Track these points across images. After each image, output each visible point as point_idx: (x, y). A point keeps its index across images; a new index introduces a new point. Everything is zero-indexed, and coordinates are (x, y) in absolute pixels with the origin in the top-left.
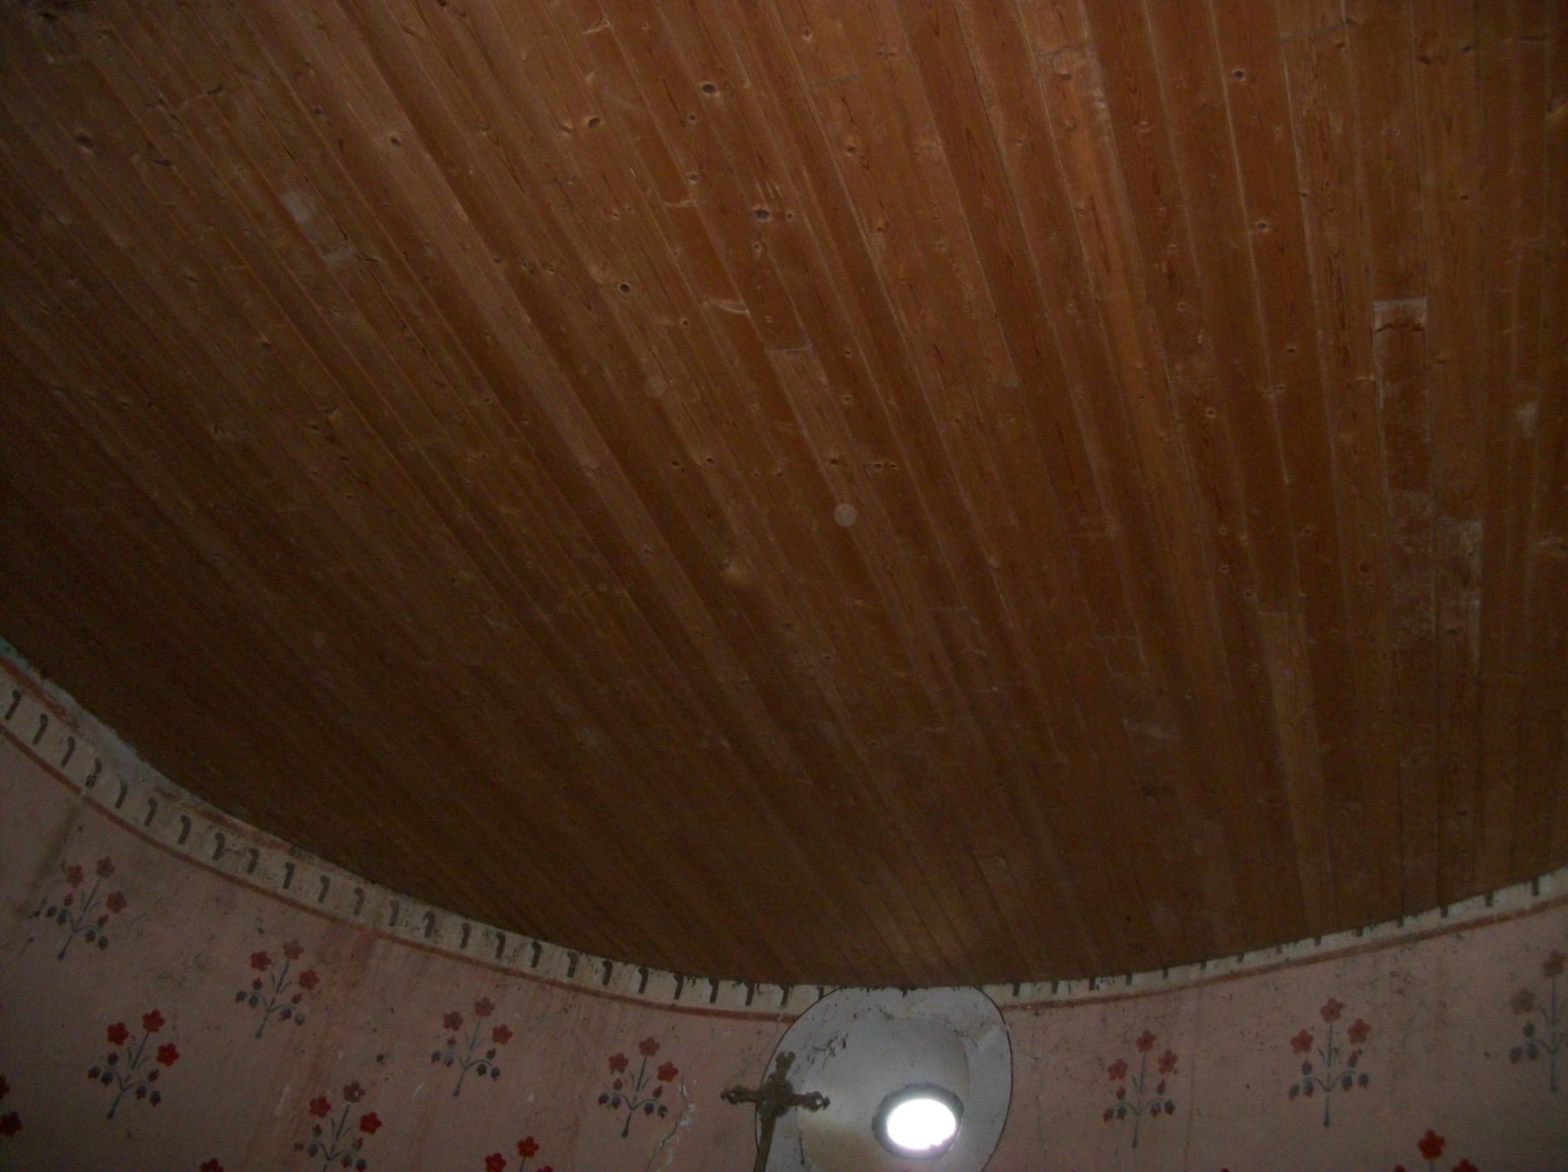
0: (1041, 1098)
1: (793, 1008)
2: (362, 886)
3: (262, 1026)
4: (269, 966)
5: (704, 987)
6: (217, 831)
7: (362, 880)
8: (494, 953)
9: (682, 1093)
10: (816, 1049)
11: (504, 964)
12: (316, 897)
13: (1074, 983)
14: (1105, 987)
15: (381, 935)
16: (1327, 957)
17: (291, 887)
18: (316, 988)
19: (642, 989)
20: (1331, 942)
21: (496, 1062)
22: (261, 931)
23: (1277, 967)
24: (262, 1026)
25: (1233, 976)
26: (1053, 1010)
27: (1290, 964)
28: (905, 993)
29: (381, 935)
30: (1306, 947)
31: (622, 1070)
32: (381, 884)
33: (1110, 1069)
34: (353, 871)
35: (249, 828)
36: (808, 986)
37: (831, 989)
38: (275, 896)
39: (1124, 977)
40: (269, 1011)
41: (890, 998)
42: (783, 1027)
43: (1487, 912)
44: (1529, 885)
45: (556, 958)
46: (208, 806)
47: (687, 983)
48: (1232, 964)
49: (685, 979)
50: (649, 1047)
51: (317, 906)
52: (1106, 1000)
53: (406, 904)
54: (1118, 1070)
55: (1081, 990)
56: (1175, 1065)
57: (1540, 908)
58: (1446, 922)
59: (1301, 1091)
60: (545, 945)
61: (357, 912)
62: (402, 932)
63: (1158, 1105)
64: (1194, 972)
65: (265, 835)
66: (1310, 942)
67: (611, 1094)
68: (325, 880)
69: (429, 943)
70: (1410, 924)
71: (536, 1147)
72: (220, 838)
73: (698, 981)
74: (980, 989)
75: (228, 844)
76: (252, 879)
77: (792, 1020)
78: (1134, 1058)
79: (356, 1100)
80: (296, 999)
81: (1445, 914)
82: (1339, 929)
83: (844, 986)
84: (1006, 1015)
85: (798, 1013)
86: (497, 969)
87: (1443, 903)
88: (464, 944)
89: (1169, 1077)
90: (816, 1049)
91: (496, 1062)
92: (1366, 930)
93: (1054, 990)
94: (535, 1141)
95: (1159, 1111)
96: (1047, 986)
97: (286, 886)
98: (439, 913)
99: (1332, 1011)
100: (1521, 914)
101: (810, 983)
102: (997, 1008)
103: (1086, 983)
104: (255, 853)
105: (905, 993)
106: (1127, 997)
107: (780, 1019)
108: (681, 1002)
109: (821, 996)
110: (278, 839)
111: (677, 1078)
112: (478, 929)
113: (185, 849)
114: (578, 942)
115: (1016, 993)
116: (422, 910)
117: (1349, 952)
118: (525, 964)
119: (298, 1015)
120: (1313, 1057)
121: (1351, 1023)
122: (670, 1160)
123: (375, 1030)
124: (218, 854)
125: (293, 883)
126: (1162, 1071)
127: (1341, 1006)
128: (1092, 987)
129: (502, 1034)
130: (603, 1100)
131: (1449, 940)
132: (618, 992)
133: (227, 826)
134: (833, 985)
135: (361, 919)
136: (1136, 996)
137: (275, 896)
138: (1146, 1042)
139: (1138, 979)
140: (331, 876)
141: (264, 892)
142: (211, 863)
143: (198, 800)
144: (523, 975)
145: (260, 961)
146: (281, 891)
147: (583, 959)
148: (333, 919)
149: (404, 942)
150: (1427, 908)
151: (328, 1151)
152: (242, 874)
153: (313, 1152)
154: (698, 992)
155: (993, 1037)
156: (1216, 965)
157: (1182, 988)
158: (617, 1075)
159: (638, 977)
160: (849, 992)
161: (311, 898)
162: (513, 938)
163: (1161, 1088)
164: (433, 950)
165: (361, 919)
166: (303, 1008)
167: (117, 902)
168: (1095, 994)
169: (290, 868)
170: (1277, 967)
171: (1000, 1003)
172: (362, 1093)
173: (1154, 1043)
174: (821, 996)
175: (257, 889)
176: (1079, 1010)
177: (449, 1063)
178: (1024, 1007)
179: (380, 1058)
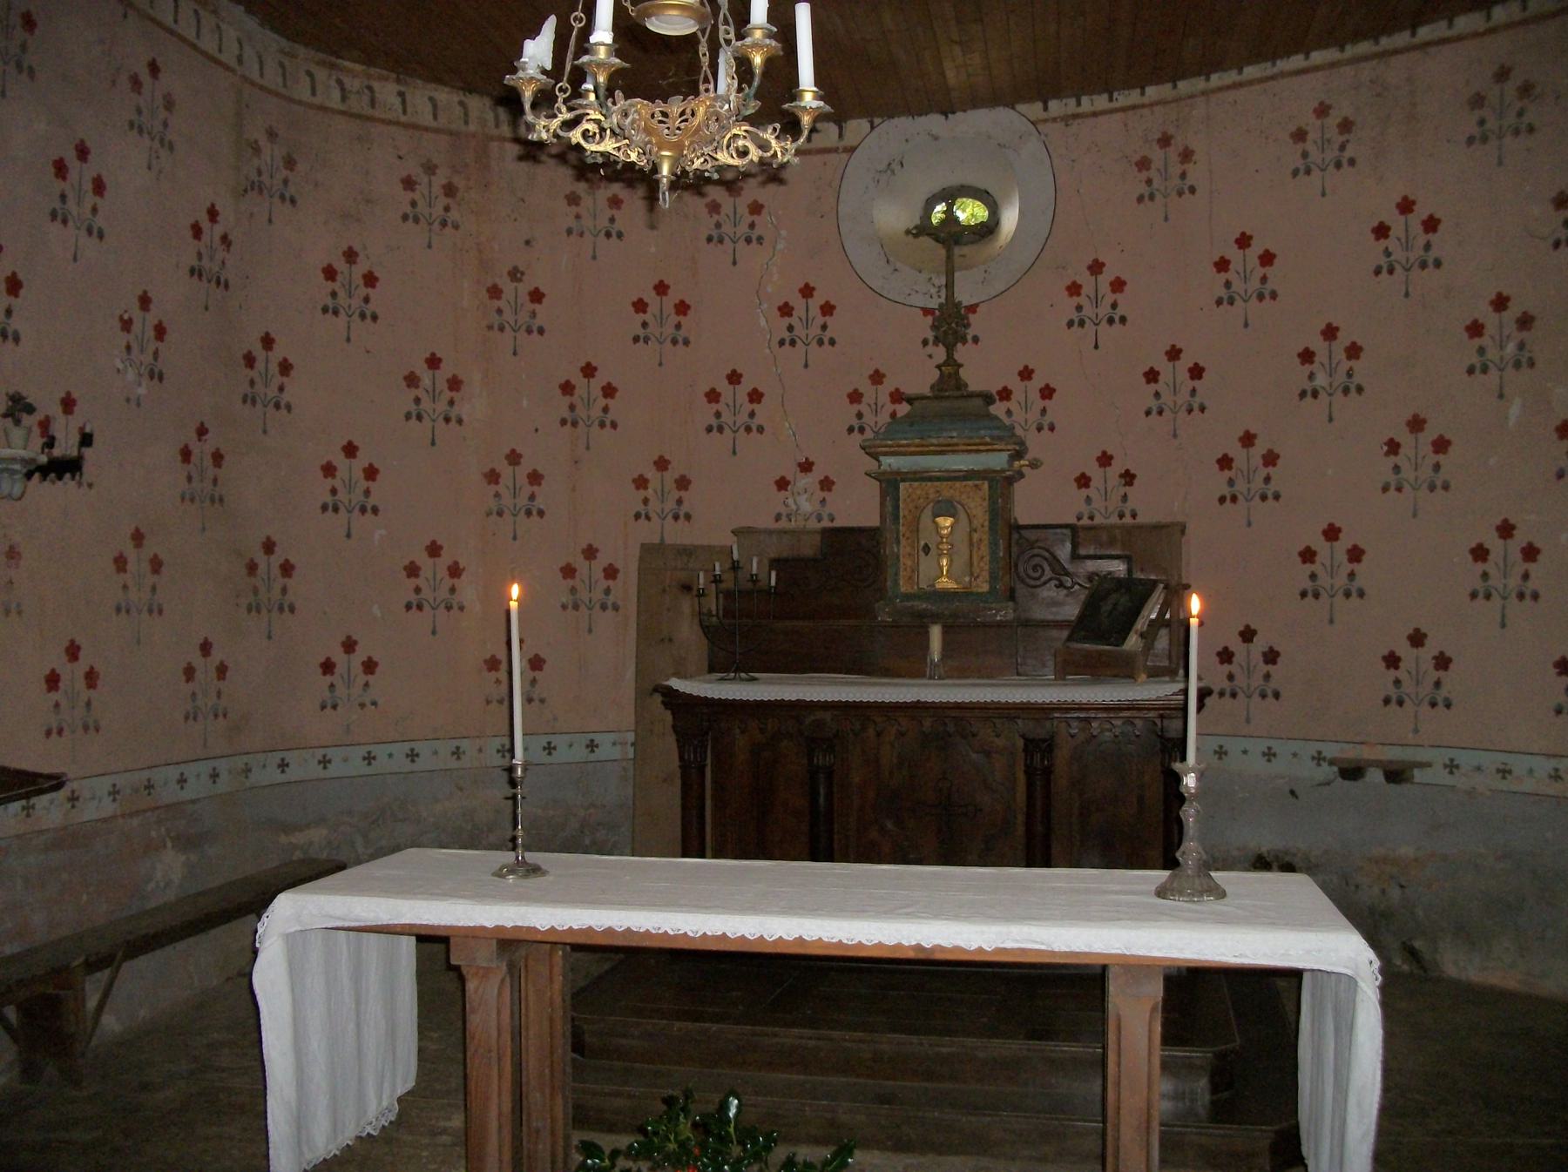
0: (1081, 191)
1: (850, 139)
2: (463, 98)
3: (430, 238)
4: (417, 186)
6: (334, 77)
7: (461, 93)
9: (772, 223)
12: (431, 117)
13: (1094, 97)
14: (1125, 98)
15: (492, 138)
16: (1316, 68)
17: (318, 93)
18: (459, 195)
20: (1318, 57)
22: (400, 158)
23: (1273, 78)
24: (430, 238)
26: (1080, 121)
27: (1283, 75)
29: (492, 138)
30: (1297, 61)
31: (718, 213)
32: (478, 93)
33: (1137, 164)
34: (453, 87)
35: (358, 67)
36: (859, 120)
37: (879, 120)
38: (397, 123)
39: (1138, 90)
40: (430, 224)
41: (934, 122)
42: (845, 156)
43: (1448, 33)
46: (321, 56)
48: (1231, 77)
51: (434, 124)
52: (1124, 109)
54: (1143, 164)
55: (1101, 102)
56: (1194, 158)
58: (1416, 40)
59: (1302, 172)
61: (466, 123)
63: (1182, 189)
64: (1199, 84)
65: (373, 71)
66: (1301, 57)
67: (715, 233)
68: (431, 99)
71: (668, 287)
72: (340, 82)
74: (1013, 108)
76: (377, 113)
77: (851, 150)
78: (1157, 155)
79: (520, 280)
80: (447, 209)
81: (1413, 34)
82: (1326, 46)
83: (891, 117)
84: (1040, 127)
85: (855, 144)
89: (1189, 167)
91: (618, 226)
93: (1079, 104)
94: (666, 282)
95: (1184, 193)
96: (1072, 102)
97: (405, 112)
99: (1322, 111)
100: (1476, 35)
101: (860, 117)
102: (1032, 123)
104: (370, 88)
105: (947, 117)
106: (1143, 106)
107: (841, 150)
110: (385, 72)
111: (765, 211)
113: (317, 100)
115: (1046, 109)
117: (1333, 65)
119: (453, 222)
120: (1309, 146)
121: (1338, 120)
122: (775, 277)
123: (515, 220)
124: (344, 98)
125: (409, 110)
126: (1182, 163)
127: (1329, 107)
128: (1111, 100)
130: (710, 239)
131: (1416, 55)
133: (341, 70)
134: (881, 116)
135: (472, 128)
136: (1151, 105)
137: (397, 123)
138: (1165, 141)
140: (466, 101)
141: (389, 123)
142: (342, 107)
143: (313, 52)
145: (409, 184)
146: (403, 119)
148: (451, 133)
150: (1401, 29)
151: (513, 324)
152: (369, 111)
153: (502, 329)
155: (1033, 146)
156: (1220, 78)
157: (1192, 96)
158: (716, 217)
160: (896, 121)
161: (426, 118)
163: (1183, 176)
166: (454, 215)
167: (290, 163)
168: (1115, 105)
169: (401, 94)
170: (1273, 78)
172: (522, 274)
173: (1173, 142)
174: (872, 128)
175: (383, 121)
176: (1101, 119)
177: (581, 234)
178: (1054, 120)
179: (528, 243)
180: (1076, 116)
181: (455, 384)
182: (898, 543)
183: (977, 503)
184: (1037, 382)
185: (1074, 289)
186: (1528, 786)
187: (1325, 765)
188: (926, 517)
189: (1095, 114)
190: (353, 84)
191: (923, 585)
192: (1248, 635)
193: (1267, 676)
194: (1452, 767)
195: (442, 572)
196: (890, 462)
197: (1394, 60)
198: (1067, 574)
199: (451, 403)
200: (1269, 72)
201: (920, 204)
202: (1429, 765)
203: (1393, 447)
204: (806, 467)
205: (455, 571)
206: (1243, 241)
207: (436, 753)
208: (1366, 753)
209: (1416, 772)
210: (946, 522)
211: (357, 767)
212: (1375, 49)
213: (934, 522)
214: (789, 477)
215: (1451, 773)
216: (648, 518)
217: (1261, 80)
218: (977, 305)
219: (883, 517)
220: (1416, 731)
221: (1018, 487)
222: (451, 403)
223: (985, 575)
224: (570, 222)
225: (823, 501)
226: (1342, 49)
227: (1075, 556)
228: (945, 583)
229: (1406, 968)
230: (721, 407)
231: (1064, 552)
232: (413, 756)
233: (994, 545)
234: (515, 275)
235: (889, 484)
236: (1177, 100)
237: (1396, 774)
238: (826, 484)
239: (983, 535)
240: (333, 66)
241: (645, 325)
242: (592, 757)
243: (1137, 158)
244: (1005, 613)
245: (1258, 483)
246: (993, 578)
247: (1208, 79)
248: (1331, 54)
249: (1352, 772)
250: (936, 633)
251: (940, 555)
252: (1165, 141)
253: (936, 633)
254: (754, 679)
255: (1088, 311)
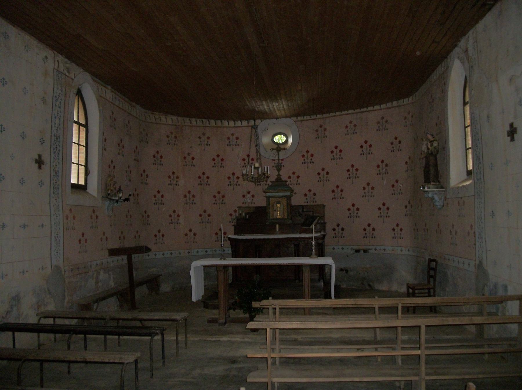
5: (239, 122)
8: (202, 124)
10: (263, 131)
11: (204, 125)
19: (228, 124)
20: (350, 111)
21: (209, 143)
25: (334, 116)
27: (344, 115)
28: (277, 120)
30: (346, 112)
38: (166, 124)
39: (316, 116)
43: (373, 109)
44: (379, 106)
45: (212, 122)
47: (236, 122)
48: (334, 114)
49: (235, 121)
50: (233, 135)
52: (313, 119)
53: (185, 119)
54: (317, 131)
55: (308, 118)
57: (381, 109)
58: (367, 110)
60: (210, 120)
61: (178, 123)
62: (186, 124)
64: (328, 115)
66: (347, 111)
67: (229, 144)
68: (172, 119)
69: (191, 125)
70: (362, 110)
72: (155, 117)
73: (238, 121)
75: (156, 118)
85: (271, 160)
86: (203, 127)
87: (367, 107)
88: (197, 124)
90: (263, 131)
92: (355, 110)
97: (167, 122)
98: (191, 119)
99: (351, 122)
100: (378, 110)
103: (309, 116)
104: (160, 117)
108: (236, 126)
109: (261, 121)
112: (198, 120)
114: (215, 118)
115: (297, 118)
116: (188, 119)
117: (353, 113)
118: (208, 125)
128: (310, 117)
129: (208, 138)
132: (225, 126)
135: (180, 124)
139: (318, 116)
141: (164, 124)
144: (208, 127)
147: (217, 121)
148: (175, 125)
149: (187, 126)
154: (238, 123)
159: (227, 122)
162: (204, 120)
164: (193, 126)
165: (180, 124)
166: (177, 142)
167: (147, 135)
171: (294, 120)
172: (190, 154)
174: (261, 121)
178: (299, 121)
179: (191, 147)
180: (303, 120)
181: (177, 177)
182: (270, 209)
183: (284, 201)
184: (296, 175)
185: (303, 156)
186: (388, 252)
187: (353, 250)
188: (275, 205)
189: (307, 120)
190: (157, 117)
191: (275, 217)
192: (338, 225)
193: (342, 233)
194: (376, 249)
195: (176, 216)
196: (268, 194)
197: (364, 113)
198: (301, 214)
199: (177, 181)
200: (341, 114)
201: (271, 136)
202: (371, 249)
203: (364, 189)
204: (249, 193)
205: (178, 216)
206: (336, 147)
207: (175, 253)
208: (361, 248)
209: (369, 251)
210: (279, 205)
211: (169, 255)
212: (360, 111)
213: (277, 205)
214: (245, 195)
215: (376, 250)
216: (216, 204)
217: (340, 115)
218: (284, 159)
219: (267, 205)
220: (369, 243)
221: (292, 198)
222: (177, 181)
223: (286, 215)
224: (199, 143)
225: (252, 200)
226: (354, 110)
227: (303, 211)
228: (279, 217)
229: (369, 288)
230: (231, 180)
231: (301, 211)
232: (171, 254)
233: (288, 209)
234: (189, 154)
235: (268, 198)
236: (323, 118)
237: (365, 251)
238: (253, 196)
239: (285, 208)
240: (153, 114)
241: (215, 163)
242: (206, 254)
243: (315, 129)
244: (289, 222)
245: (339, 195)
246: (288, 216)
247: (329, 114)
248: (352, 111)
249: (357, 251)
250: (277, 226)
251: (278, 212)
252: (321, 126)
253: (277, 226)
254: (244, 235)
255: (306, 160)
